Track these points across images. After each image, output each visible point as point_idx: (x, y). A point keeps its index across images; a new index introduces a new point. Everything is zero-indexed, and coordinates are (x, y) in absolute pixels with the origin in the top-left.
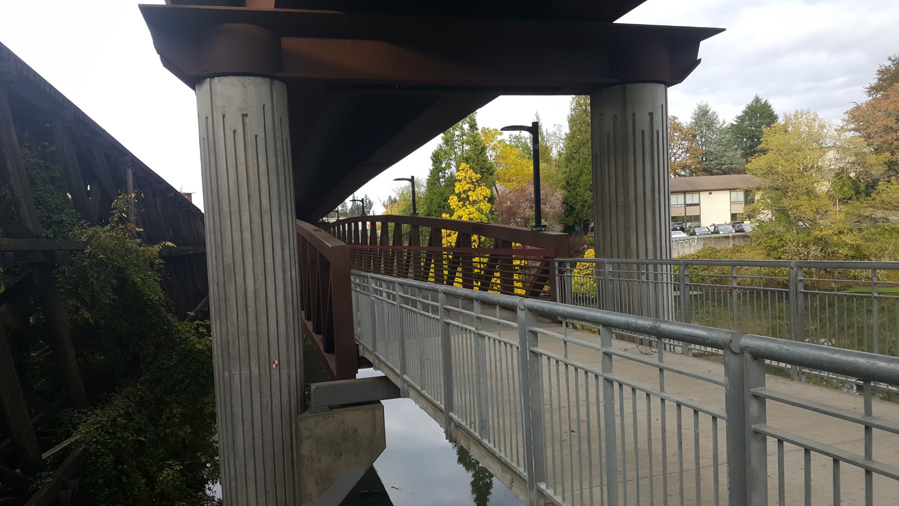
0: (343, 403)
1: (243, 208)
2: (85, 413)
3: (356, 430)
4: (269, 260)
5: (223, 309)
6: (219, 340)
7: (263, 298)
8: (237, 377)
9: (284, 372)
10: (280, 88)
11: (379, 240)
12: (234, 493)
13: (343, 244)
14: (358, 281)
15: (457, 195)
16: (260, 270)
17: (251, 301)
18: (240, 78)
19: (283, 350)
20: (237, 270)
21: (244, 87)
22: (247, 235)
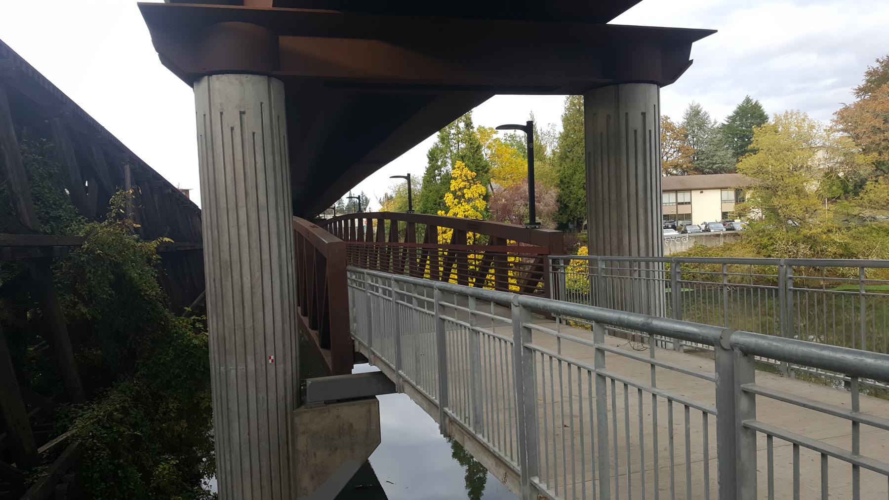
0: (339, 398)
1: (240, 204)
2: (82, 408)
3: (351, 425)
4: (266, 256)
5: (220, 304)
7: (259, 294)
8: (233, 372)
9: (280, 367)
10: (277, 86)
13: (339, 240)
14: (354, 277)
16: (257, 266)
17: (247, 296)
18: (238, 76)
20: (234, 266)
21: (241, 83)
22: (244, 231)
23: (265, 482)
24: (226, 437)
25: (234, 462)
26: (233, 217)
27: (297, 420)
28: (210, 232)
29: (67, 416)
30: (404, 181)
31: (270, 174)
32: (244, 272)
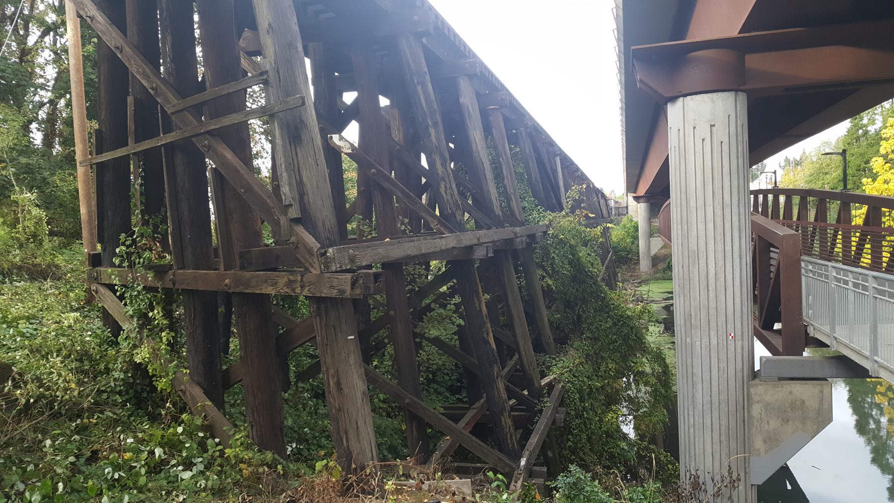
0: (791, 376)
1: (707, 204)
2: (554, 359)
3: (803, 402)
4: (728, 247)
5: (687, 287)
6: (682, 313)
7: (722, 280)
8: (698, 343)
9: (739, 344)
10: (742, 97)
11: (770, 210)
12: (692, 438)
13: (793, 232)
14: (810, 267)
15: (883, 156)
16: (720, 256)
17: (712, 282)
18: (709, 95)
19: (738, 325)
20: (701, 255)
21: (713, 101)
22: (710, 226)
23: (723, 438)
24: (691, 395)
25: (696, 418)
26: (701, 213)
27: (752, 390)
28: (680, 227)
29: (544, 363)
30: (840, 158)
31: (735, 176)
32: (709, 261)
